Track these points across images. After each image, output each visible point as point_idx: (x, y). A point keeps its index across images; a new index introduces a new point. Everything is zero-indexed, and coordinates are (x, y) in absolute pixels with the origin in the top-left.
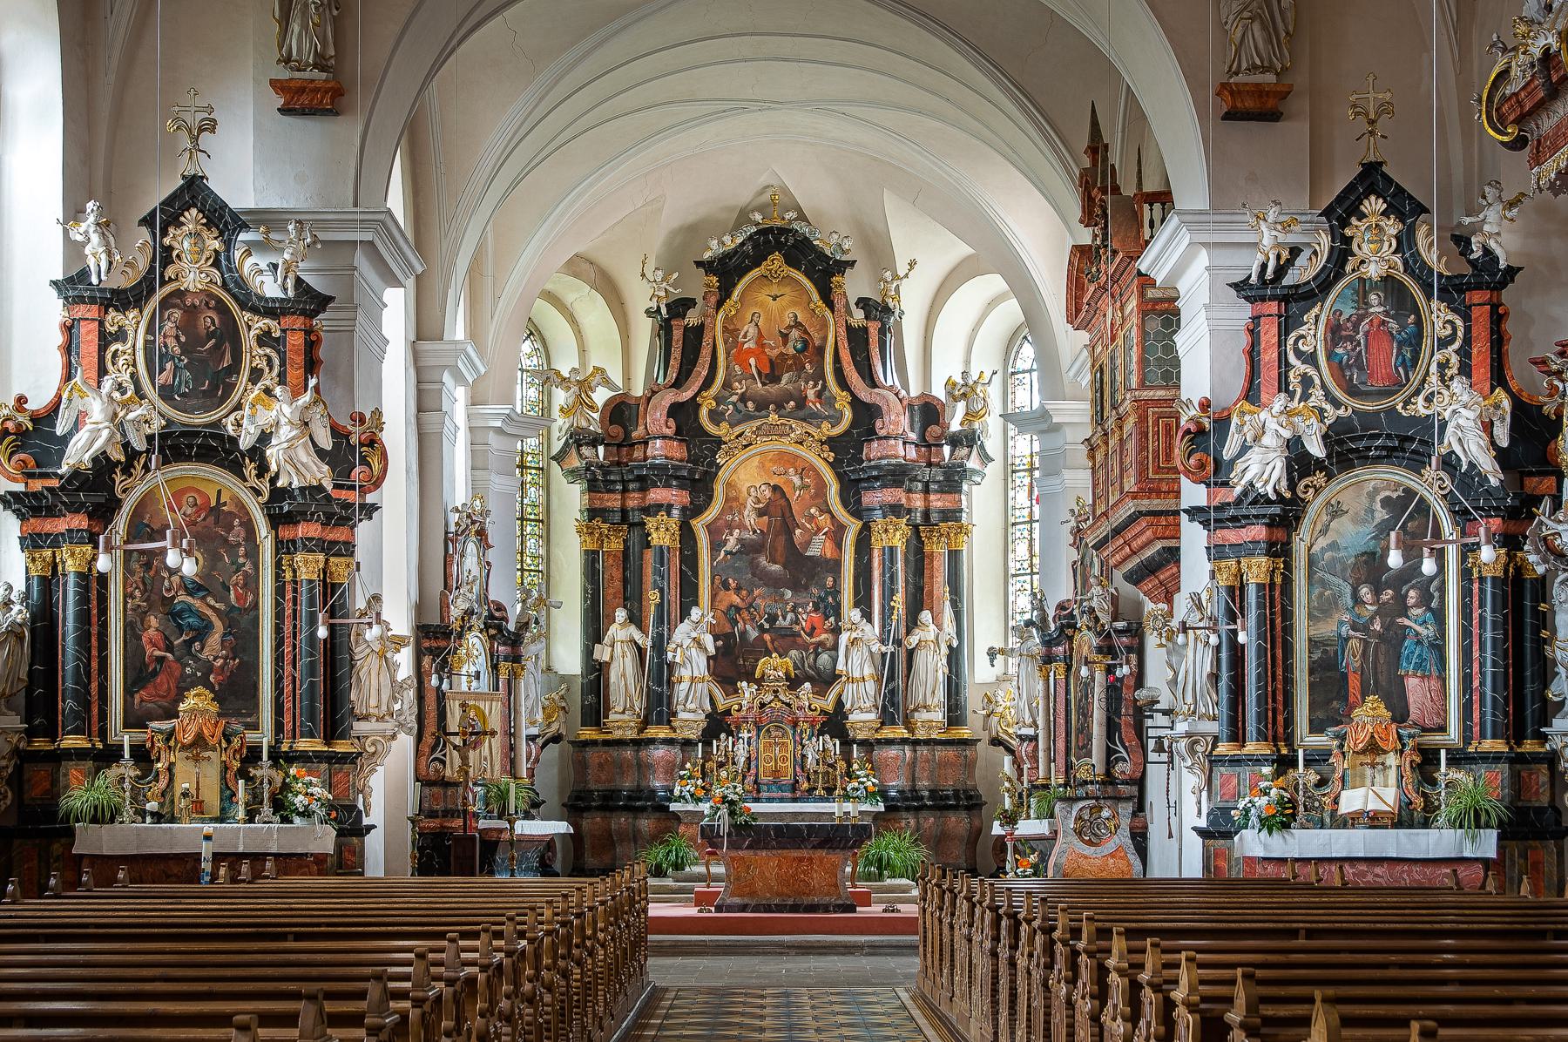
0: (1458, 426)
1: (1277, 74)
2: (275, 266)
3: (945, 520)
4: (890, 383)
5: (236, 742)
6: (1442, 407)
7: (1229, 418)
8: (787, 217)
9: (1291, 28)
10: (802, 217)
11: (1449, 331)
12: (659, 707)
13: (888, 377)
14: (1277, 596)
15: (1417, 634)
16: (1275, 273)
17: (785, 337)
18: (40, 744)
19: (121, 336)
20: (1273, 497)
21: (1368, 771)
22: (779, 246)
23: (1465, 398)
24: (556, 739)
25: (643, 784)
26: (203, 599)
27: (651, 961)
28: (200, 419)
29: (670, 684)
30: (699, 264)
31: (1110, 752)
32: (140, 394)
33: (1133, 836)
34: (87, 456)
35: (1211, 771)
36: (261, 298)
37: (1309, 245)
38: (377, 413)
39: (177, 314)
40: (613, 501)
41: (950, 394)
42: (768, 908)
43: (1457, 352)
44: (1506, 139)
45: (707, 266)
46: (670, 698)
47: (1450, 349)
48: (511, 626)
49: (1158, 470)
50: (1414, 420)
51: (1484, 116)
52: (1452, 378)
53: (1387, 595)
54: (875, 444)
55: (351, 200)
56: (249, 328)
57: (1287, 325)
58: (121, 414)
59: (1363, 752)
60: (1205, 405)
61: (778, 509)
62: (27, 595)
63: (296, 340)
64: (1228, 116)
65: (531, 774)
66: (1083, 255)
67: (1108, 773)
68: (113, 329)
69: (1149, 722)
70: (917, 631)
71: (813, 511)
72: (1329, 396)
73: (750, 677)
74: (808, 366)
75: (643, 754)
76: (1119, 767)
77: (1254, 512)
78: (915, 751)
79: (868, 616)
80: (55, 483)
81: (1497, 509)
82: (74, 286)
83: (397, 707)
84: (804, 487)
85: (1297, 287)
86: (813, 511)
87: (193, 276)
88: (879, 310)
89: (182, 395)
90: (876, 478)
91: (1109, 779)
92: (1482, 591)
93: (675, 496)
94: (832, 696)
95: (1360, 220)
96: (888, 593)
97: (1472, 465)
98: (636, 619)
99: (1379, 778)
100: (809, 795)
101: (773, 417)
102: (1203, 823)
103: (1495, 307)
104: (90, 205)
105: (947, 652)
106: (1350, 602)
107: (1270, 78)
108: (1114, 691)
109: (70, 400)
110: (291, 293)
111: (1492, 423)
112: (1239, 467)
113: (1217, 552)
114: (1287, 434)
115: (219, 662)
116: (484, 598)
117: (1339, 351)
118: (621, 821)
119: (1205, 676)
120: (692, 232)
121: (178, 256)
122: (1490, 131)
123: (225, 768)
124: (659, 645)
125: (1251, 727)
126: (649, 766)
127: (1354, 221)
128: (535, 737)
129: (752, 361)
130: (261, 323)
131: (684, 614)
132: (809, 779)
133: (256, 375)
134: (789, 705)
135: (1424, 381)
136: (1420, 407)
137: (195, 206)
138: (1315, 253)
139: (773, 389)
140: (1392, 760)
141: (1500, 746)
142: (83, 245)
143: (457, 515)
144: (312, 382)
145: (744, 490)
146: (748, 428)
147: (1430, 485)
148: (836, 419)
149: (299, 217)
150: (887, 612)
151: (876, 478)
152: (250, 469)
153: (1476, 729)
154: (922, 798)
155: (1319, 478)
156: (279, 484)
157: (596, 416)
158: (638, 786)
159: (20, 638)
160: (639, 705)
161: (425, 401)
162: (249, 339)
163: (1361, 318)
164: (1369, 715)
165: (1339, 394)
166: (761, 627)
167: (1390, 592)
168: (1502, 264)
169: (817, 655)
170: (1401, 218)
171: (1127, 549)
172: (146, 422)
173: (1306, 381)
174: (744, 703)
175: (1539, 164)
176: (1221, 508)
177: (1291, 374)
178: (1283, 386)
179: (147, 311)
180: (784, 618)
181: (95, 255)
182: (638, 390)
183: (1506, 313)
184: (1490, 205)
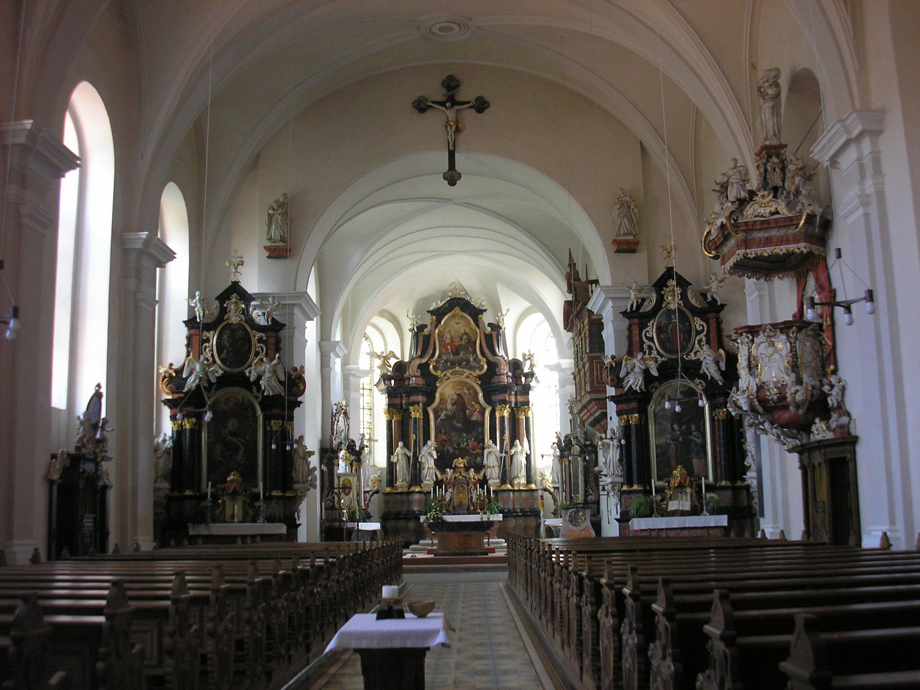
0: (706, 363)
1: (634, 236)
3: (524, 405)
4: (500, 355)
5: (249, 492)
10: (467, 294)
11: (701, 328)
12: (416, 477)
14: (642, 428)
15: (696, 442)
17: (461, 338)
18: (176, 494)
19: (208, 340)
20: (639, 391)
21: (680, 495)
22: (458, 305)
23: (708, 352)
24: (377, 492)
28: (236, 370)
30: (428, 312)
32: (214, 362)
33: (593, 524)
34: (194, 385)
37: (648, 297)
38: (302, 368)
40: (398, 401)
41: (524, 358)
42: (454, 554)
43: (704, 336)
44: (711, 255)
47: (702, 335)
48: (357, 449)
49: (598, 383)
50: (691, 361)
51: (703, 248)
52: (703, 345)
53: (684, 427)
54: (496, 377)
55: (293, 289)
56: (255, 336)
57: (643, 326)
58: (207, 369)
59: (677, 487)
60: (613, 357)
61: (460, 402)
62: (171, 438)
64: (617, 251)
66: (568, 304)
68: (205, 338)
69: (600, 479)
70: (514, 448)
71: (473, 403)
72: (659, 353)
74: (470, 349)
75: (410, 497)
76: (590, 497)
77: (632, 397)
79: (495, 442)
82: (191, 323)
86: (473, 403)
87: (234, 318)
88: (496, 328)
90: (497, 390)
91: (586, 502)
92: (719, 425)
94: (482, 474)
95: (666, 288)
96: (502, 433)
98: (407, 446)
99: (684, 497)
101: (457, 368)
102: (618, 517)
104: (197, 293)
105: (526, 456)
107: (631, 237)
110: (270, 323)
112: (626, 381)
113: (619, 413)
114: (643, 367)
115: (243, 462)
116: (347, 438)
117: (662, 336)
118: (402, 523)
120: (426, 300)
121: (229, 311)
122: (706, 253)
123: (244, 502)
124: (415, 456)
125: (635, 479)
126: (412, 502)
127: (665, 289)
128: (368, 492)
129: (449, 347)
130: (259, 335)
131: (425, 443)
132: (474, 506)
133: (257, 354)
134: (465, 477)
135: (693, 347)
136: (692, 357)
137: (236, 292)
138: (651, 301)
139: (457, 358)
140: (689, 490)
141: (729, 484)
142: (194, 307)
144: (277, 356)
146: (449, 373)
147: (698, 386)
148: (481, 368)
150: (502, 441)
152: (255, 389)
153: (719, 477)
154: (517, 512)
155: (657, 384)
156: (265, 394)
157: (391, 369)
160: (408, 478)
161: (325, 364)
162: (254, 341)
163: (669, 324)
165: (662, 352)
168: (719, 304)
170: (681, 287)
171: (589, 413)
173: (650, 348)
174: (448, 477)
175: (724, 264)
176: (621, 395)
178: (642, 349)
179: (217, 332)
182: (407, 359)
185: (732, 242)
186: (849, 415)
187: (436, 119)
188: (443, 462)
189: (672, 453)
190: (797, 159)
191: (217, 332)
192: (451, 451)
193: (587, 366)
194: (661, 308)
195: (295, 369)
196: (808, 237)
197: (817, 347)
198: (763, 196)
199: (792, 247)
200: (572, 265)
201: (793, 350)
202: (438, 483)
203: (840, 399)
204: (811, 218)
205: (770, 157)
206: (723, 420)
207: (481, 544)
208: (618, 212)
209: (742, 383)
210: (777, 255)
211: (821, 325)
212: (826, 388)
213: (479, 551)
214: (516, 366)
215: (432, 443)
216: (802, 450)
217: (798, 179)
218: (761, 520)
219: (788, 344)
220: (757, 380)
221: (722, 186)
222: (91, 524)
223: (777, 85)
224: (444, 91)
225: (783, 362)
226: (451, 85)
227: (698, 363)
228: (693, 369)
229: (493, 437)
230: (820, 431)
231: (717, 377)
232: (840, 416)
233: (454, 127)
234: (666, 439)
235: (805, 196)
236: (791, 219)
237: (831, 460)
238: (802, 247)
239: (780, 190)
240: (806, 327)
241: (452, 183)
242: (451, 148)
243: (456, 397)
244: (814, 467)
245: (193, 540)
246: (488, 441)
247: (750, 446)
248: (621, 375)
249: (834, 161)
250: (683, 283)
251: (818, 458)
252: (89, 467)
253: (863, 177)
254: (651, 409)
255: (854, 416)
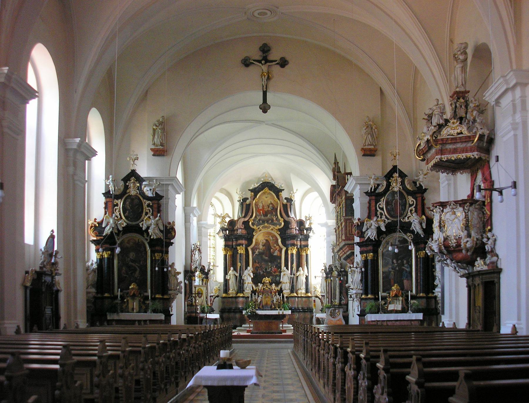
0: (414, 224)
1: (374, 146)
2: (151, 189)
4: (292, 217)
5: (142, 295)
6: (411, 220)
7: (364, 222)
8: (269, 179)
9: (377, 136)
10: (272, 179)
11: (412, 203)
12: (241, 288)
13: (292, 215)
14: (375, 262)
15: (406, 270)
16: (374, 190)
17: (269, 206)
18: (99, 295)
19: (117, 205)
20: (374, 240)
21: (395, 301)
23: (416, 217)
24: (218, 296)
25: (237, 306)
26: (135, 263)
27: (233, 344)
28: (134, 223)
29: (243, 284)
31: (340, 298)
32: (121, 218)
35: (361, 301)
36: (148, 196)
38: (174, 222)
39: (129, 200)
40: (230, 243)
41: (306, 219)
42: (262, 333)
45: (252, 191)
46: (243, 287)
47: (413, 207)
48: (206, 271)
49: (350, 234)
50: (405, 222)
51: (416, 154)
52: (413, 213)
54: (289, 230)
55: (168, 175)
56: (145, 203)
57: (377, 201)
58: (117, 222)
59: (394, 296)
60: (359, 219)
61: (267, 245)
62: (97, 262)
63: (156, 206)
64: (364, 155)
65: (212, 304)
67: (340, 303)
68: (115, 204)
69: (349, 291)
70: (298, 272)
72: (386, 217)
73: (261, 283)
74: (274, 213)
75: (237, 300)
76: (343, 302)
78: (298, 299)
80: (102, 238)
81: (423, 242)
82: (107, 194)
83: (178, 288)
84: (273, 240)
85: (379, 193)
87: (133, 192)
88: (289, 200)
89: (131, 218)
90: (289, 238)
91: (340, 304)
93: (244, 242)
95: (392, 178)
96: (292, 263)
97: (417, 232)
98: (235, 269)
99: (398, 303)
100: (275, 309)
101: (266, 224)
102: (359, 313)
103: (423, 197)
104: (110, 176)
105: (305, 277)
106: (391, 263)
107: (372, 147)
108: (341, 286)
109: (106, 219)
110: (154, 195)
111: (422, 223)
113: (361, 253)
114: (377, 226)
115: (138, 278)
116: (200, 264)
117: (389, 207)
118: (232, 315)
119: (359, 280)
120: (248, 183)
121: (130, 187)
123: (140, 301)
124: (240, 276)
125: (369, 292)
128: (212, 296)
129: (261, 212)
130: (148, 202)
131: (246, 268)
132: (274, 305)
133: (147, 214)
134: (270, 289)
135: (407, 214)
136: (406, 220)
139: (266, 218)
140: (401, 298)
141: (424, 295)
142: (109, 185)
143: (194, 246)
145: (260, 241)
146: (261, 227)
147: (409, 237)
149: (156, 179)
150: (292, 268)
151: (289, 238)
152: (145, 235)
153: (419, 291)
154: (300, 309)
155: (384, 236)
156: (151, 238)
157: (226, 224)
158: (236, 307)
159: (95, 272)
160: (236, 289)
162: (145, 206)
164: (395, 288)
165: (388, 217)
166: (263, 271)
167: (400, 261)
168: (424, 188)
169: (276, 277)
170: (401, 178)
172: (123, 224)
173: (381, 214)
174: (260, 288)
175: (428, 164)
176: (363, 242)
177: (378, 213)
179: (123, 200)
180: (269, 269)
181: (111, 188)
182: (236, 219)
183: (425, 199)
184: (421, 175)
185: (433, 151)
186: (497, 256)
187: (256, 71)
188: (257, 280)
189: (392, 276)
190: (475, 100)
191: (123, 200)
192: (262, 273)
193: (343, 224)
194: (389, 190)
195: (169, 223)
196: (479, 149)
197: (481, 215)
198: (453, 123)
199: (469, 155)
200: (336, 163)
201: (466, 217)
202: (254, 292)
203: (492, 247)
204: (481, 137)
205: (459, 98)
206: (423, 258)
207: (278, 327)
208: (365, 131)
209: (435, 236)
210: (460, 159)
211: (484, 202)
212: (485, 240)
213: (277, 331)
214: (301, 223)
215: (250, 268)
216: (468, 276)
217: (475, 113)
218: (442, 316)
219: (464, 213)
220: (444, 234)
221: (429, 116)
222: (50, 312)
223: (466, 53)
224: (261, 53)
225: (460, 224)
226: (265, 49)
227: (410, 224)
228: (406, 227)
229: (286, 266)
230: (480, 265)
231: (421, 232)
232: (492, 256)
233: (266, 77)
234: (389, 268)
235: (479, 123)
236: (469, 137)
237: (485, 282)
238: (475, 155)
239: (464, 119)
240: (475, 203)
241: (265, 111)
242: (265, 90)
243: (265, 241)
244: (475, 286)
245: (110, 322)
246: (283, 268)
247: (438, 273)
248: (364, 230)
249: (497, 101)
250: (402, 175)
251: (478, 281)
252: (48, 279)
253: (515, 112)
254: (380, 250)
255: (500, 257)
